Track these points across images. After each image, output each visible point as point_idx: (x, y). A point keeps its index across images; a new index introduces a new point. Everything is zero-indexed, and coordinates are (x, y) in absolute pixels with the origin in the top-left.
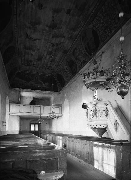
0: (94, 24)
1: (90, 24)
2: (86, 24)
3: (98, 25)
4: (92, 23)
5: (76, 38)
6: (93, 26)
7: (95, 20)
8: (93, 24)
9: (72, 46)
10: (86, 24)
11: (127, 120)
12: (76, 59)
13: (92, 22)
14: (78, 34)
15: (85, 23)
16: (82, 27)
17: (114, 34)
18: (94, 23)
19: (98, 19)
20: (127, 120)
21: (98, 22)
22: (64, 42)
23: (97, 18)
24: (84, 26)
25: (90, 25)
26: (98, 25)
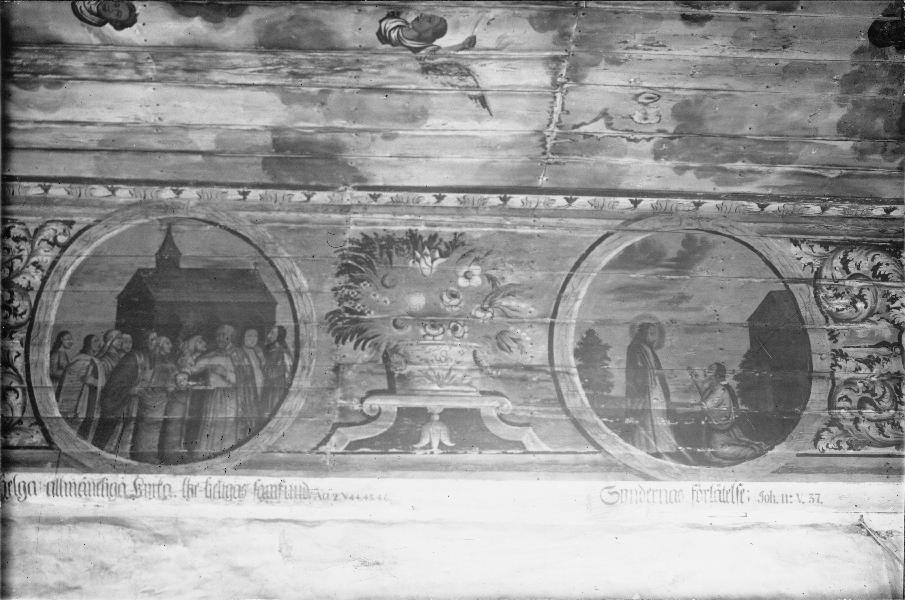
0: (826, 272)
1: (796, 243)
2: (774, 206)
3: (853, 303)
4: (818, 249)
5: (571, 193)
6: (808, 274)
7: (862, 261)
8: (823, 259)
9: (451, 199)
10: (774, 206)
11: (74, 150)
12: (348, 325)
13: (825, 244)
14: (636, 195)
15: (777, 199)
16: (721, 190)
17: (511, 442)
18: (837, 263)
19: (885, 278)
20: (74, 150)
21: (869, 295)
22: (482, 101)
23: (883, 270)
24: (754, 206)
25: (794, 249)
26: (853, 303)
